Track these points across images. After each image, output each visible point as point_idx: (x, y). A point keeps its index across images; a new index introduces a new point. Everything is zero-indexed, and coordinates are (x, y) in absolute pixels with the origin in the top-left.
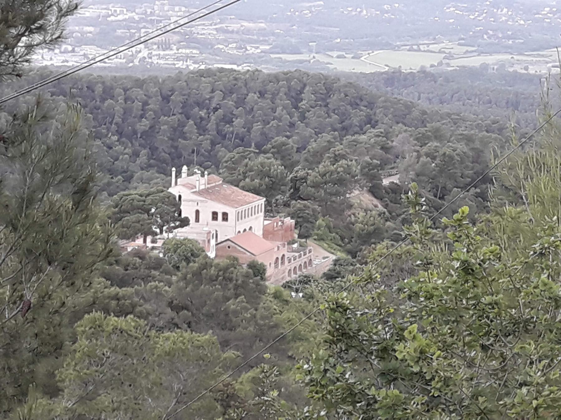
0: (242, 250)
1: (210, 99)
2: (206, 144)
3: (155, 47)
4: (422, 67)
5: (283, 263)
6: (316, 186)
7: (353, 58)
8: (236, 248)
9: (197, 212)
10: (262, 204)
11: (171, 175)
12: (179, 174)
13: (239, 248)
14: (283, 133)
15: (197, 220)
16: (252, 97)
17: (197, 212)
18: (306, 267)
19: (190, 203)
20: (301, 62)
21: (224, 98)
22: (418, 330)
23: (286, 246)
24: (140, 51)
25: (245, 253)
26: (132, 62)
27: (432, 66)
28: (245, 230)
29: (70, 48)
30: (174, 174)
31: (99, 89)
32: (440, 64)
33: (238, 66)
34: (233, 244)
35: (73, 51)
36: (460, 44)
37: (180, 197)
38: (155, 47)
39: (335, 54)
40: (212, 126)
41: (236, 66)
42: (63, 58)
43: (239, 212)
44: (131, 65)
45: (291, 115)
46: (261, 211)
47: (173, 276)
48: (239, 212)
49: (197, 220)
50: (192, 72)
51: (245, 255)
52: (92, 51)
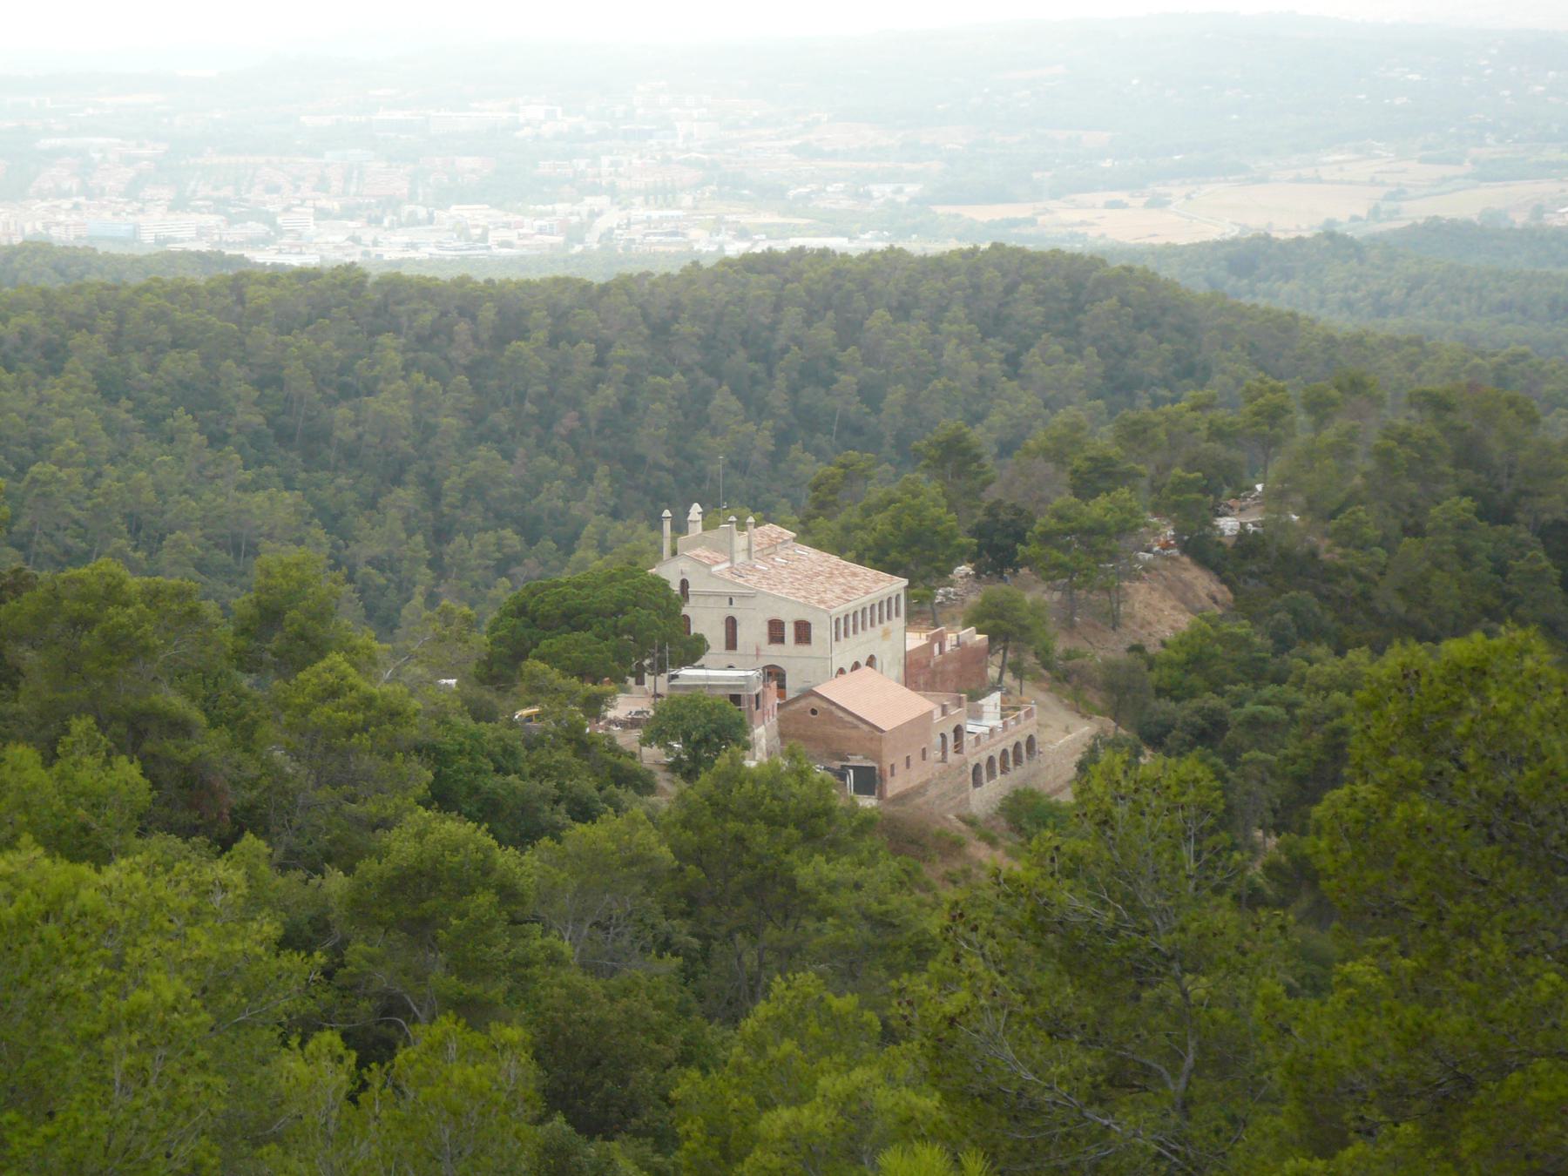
0: (850, 719)
1: (773, 328)
2: (764, 441)
3: (638, 200)
4: (1330, 222)
5: (958, 748)
6: (1047, 538)
7: (1148, 205)
8: (831, 713)
9: (731, 623)
10: (898, 596)
11: (661, 529)
12: (680, 527)
13: (841, 714)
14: (966, 411)
15: (731, 643)
16: (879, 318)
17: (731, 623)
18: (1018, 760)
19: (712, 600)
20: (1014, 223)
21: (808, 323)
22: (227, 954)
23: (965, 704)
24: (599, 214)
25: (856, 727)
26: (581, 241)
27: (1354, 219)
28: (856, 666)
29: (422, 213)
30: (667, 525)
31: (488, 313)
32: (1375, 213)
33: (851, 239)
34: (825, 705)
35: (430, 220)
36: (1423, 160)
37: (684, 584)
38: (638, 200)
39: (1101, 197)
40: (777, 397)
41: (845, 240)
42: (406, 239)
43: (838, 620)
44: (578, 248)
45: (980, 358)
46: (897, 614)
47: (1259, 910)
48: (838, 620)
49: (731, 643)
50: (728, 263)
51: (854, 733)
52: (475, 214)
